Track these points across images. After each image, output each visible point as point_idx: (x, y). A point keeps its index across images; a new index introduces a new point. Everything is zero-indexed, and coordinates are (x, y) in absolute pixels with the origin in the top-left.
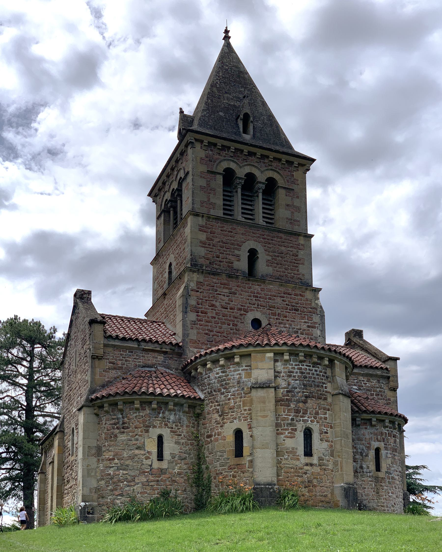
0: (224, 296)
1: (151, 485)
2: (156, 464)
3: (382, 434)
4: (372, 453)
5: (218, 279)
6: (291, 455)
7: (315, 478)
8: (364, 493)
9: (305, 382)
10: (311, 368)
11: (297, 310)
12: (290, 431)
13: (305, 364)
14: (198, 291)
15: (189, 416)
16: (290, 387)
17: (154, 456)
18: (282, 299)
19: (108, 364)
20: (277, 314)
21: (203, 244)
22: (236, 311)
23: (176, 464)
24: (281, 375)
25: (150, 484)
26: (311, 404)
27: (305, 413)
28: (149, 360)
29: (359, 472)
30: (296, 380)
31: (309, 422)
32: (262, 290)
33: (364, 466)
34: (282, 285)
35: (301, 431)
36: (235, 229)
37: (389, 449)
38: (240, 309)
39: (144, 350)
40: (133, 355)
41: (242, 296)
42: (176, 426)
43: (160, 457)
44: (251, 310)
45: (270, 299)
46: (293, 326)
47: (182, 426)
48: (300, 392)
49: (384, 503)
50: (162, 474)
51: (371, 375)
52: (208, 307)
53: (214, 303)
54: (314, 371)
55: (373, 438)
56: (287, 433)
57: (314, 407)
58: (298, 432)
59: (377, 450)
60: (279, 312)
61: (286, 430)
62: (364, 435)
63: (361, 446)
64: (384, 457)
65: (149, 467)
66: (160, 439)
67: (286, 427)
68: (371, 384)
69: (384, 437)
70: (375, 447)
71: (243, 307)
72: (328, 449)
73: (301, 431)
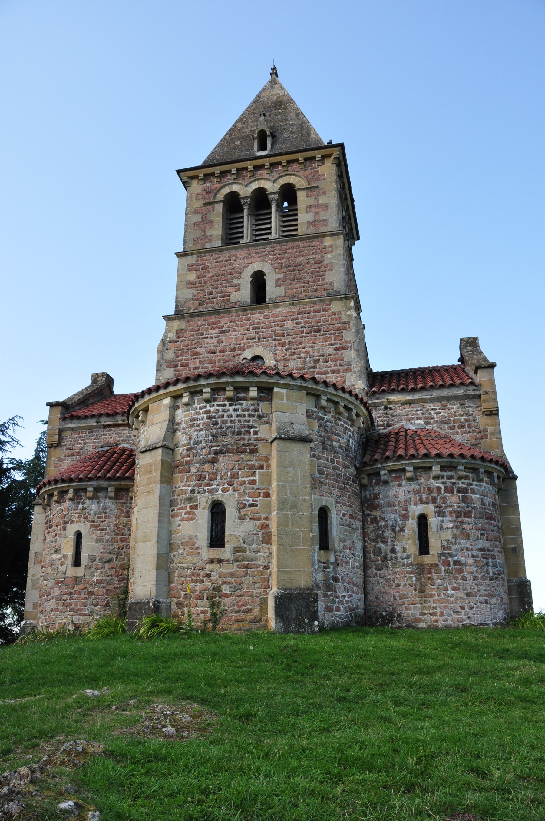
0: (212, 338)
1: (64, 600)
2: (72, 571)
3: (430, 490)
4: (412, 525)
5: (204, 320)
6: (187, 548)
7: (225, 583)
8: (397, 595)
9: (214, 431)
10: (227, 407)
11: (319, 330)
12: (188, 509)
13: (215, 404)
14: (177, 341)
15: (120, 503)
16: (192, 442)
17: (69, 561)
18: (295, 321)
19: (65, 451)
20: (287, 343)
21: (192, 285)
22: (228, 353)
23: (96, 569)
24: (181, 427)
25: (63, 598)
26: (223, 464)
27: (213, 477)
28: (111, 438)
29: (389, 558)
30: (201, 430)
31: (220, 492)
32: (265, 317)
33: (398, 548)
34: (293, 304)
35: (204, 509)
36: (234, 255)
37: (447, 513)
38: (234, 350)
39: (105, 427)
40: (93, 436)
41: (237, 333)
42: (98, 518)
43: (77, 562)
44: (249, 347)
45: (277, 326)
46: (311, 354)
47: (109, 517)
48: (205, 447)
49: (435, 608)
50: (76, 584)
51: (448, 399)
52: (189, 357)
53: (198, 350)
54: (231, 412)
55: (412, 499)
56: (183, 514)
57: (230, 467)
58: (200, 509)
59: (422, 520)
60: (290, 339)
61: (182, 508)
62: (396, 496)
63: (393, 516)
64: (435, 530)
65: (63, 576)
66: (79, 536)
67: (183, 505)
68: (449, 411)
69: (434, 494)
70: (417, 514)
71: (237, 346)
72: (255, 532)
73: (204, 509)
